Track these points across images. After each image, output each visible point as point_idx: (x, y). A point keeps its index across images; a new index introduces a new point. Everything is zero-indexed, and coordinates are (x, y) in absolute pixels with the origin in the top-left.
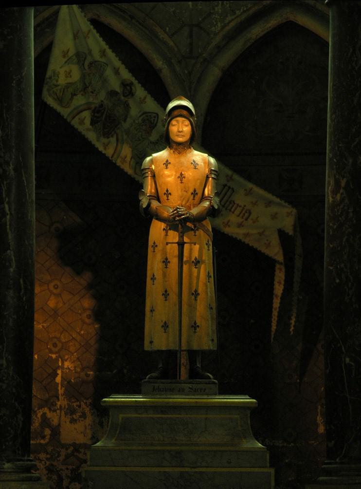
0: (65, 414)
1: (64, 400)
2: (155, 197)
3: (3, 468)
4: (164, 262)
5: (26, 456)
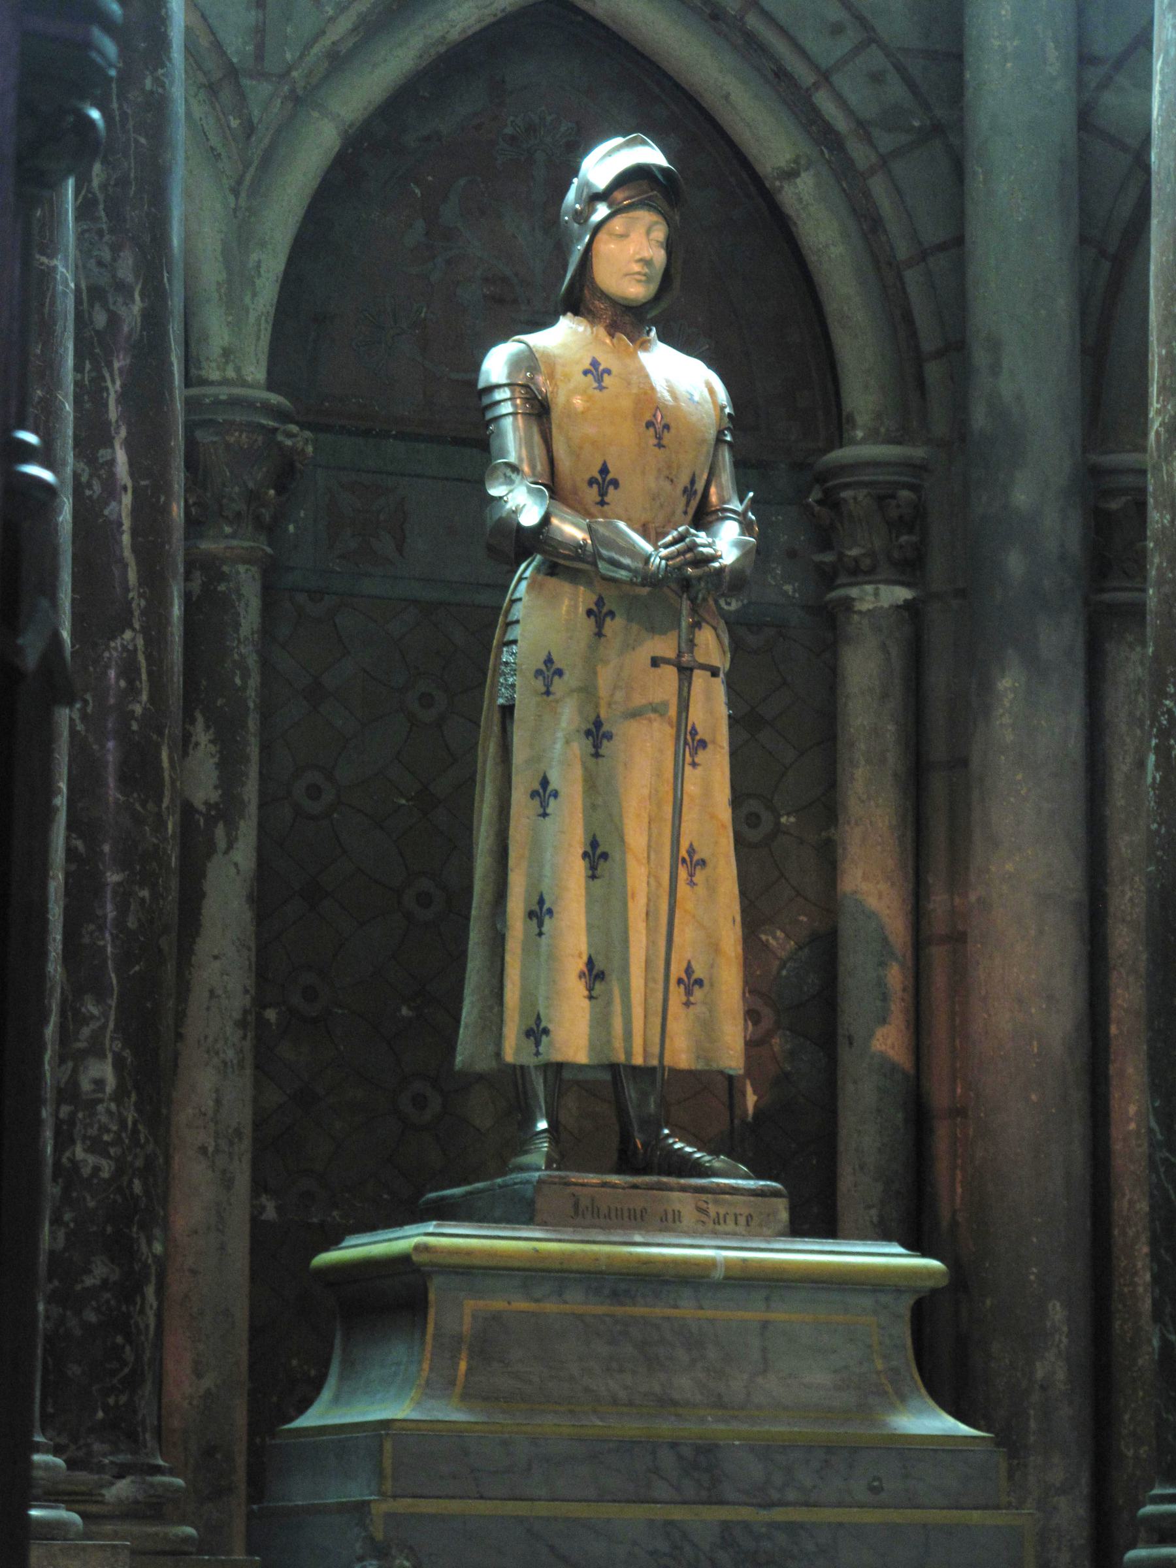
4: (588, 733)
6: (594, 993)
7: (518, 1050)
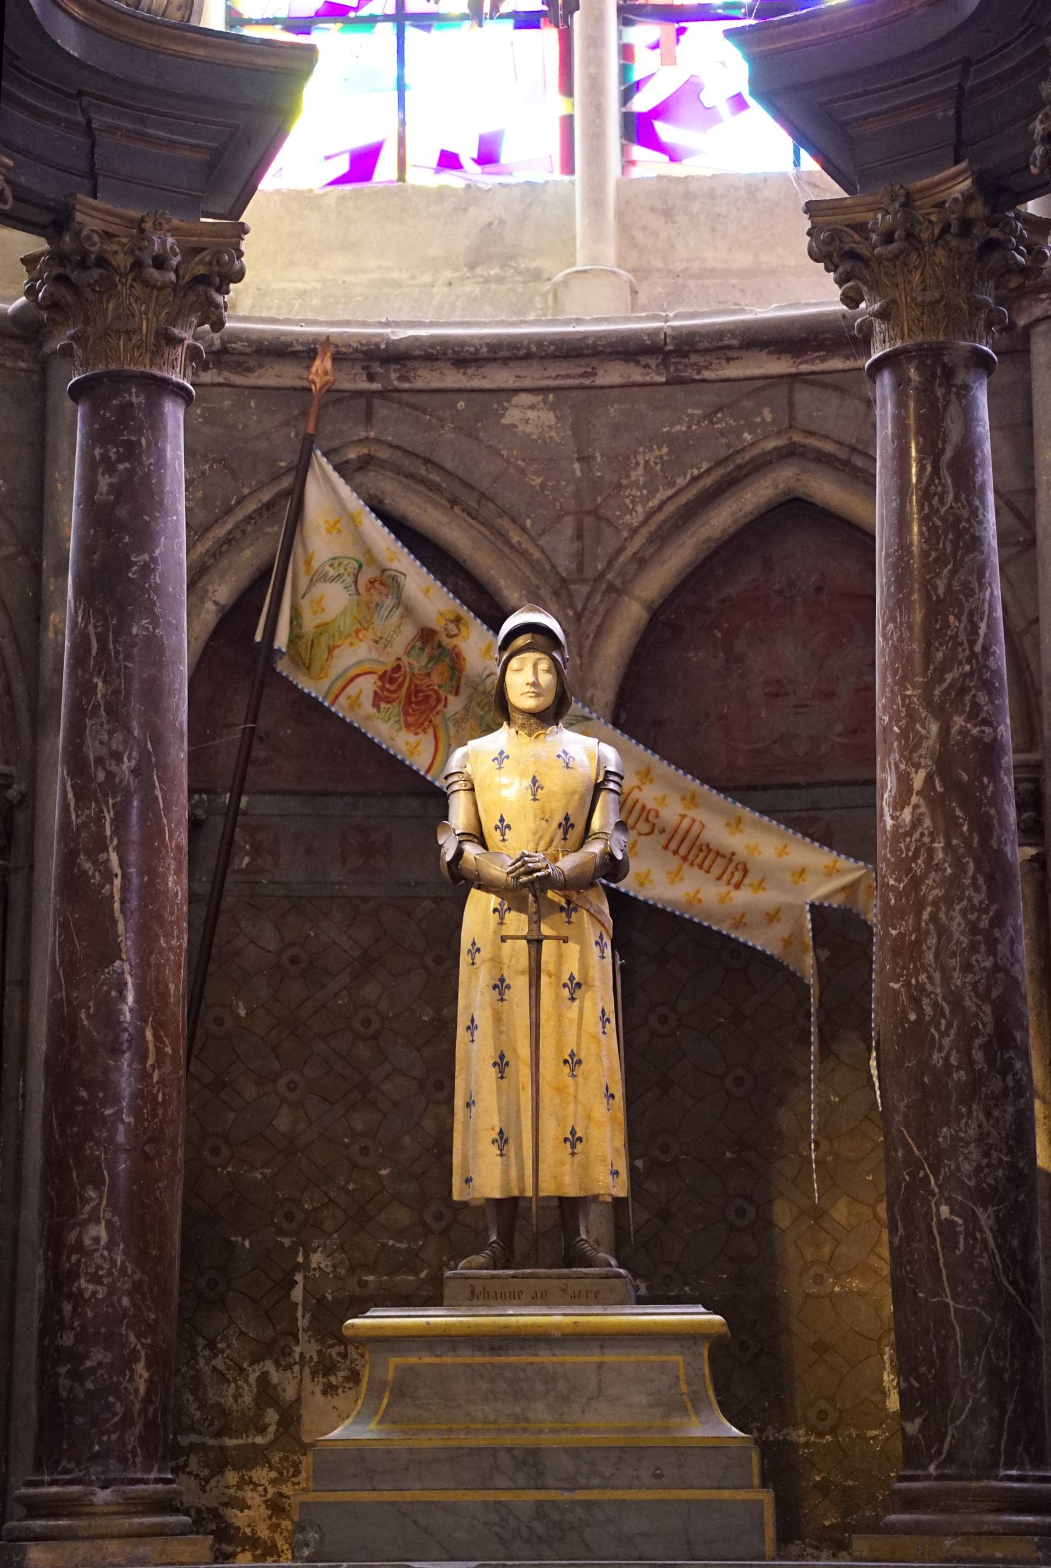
0: (311, 1373)
1: (309, 1342)
2: (475, 837)
3: (92, 1505)
4: (495, 987)
5: (155, 1470)
6: (504, 1152)
7: (461, 1193)
